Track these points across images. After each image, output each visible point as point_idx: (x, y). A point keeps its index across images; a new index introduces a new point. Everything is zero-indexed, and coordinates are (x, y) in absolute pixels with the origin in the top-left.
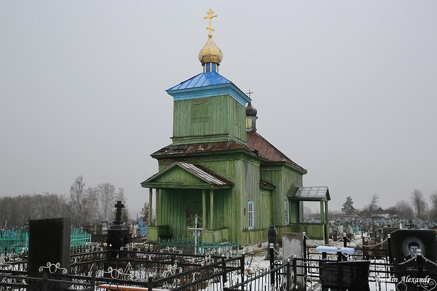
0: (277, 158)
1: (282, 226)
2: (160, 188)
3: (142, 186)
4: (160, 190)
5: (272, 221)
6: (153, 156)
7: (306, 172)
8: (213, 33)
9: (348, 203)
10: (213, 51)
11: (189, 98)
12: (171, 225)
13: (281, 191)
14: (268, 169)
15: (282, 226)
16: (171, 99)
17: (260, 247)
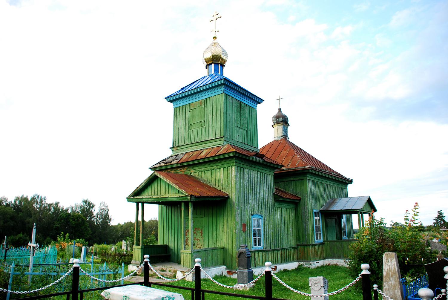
0: (299, 164)
1: (309, 245)
2: (140, 202)
3: (128, 201)
4: (139, 204)
5: (298, 239)
6: (149, 168)
7: (351, 182)
8: (217, 35)
9: (441, 217)
10: (217, 51)
11: (186, 103)
12: (170, 245)
13: (308, 204)
14: (292, 179)
15: (309, 245)
16: (171, 105)
17: (275, 270)
